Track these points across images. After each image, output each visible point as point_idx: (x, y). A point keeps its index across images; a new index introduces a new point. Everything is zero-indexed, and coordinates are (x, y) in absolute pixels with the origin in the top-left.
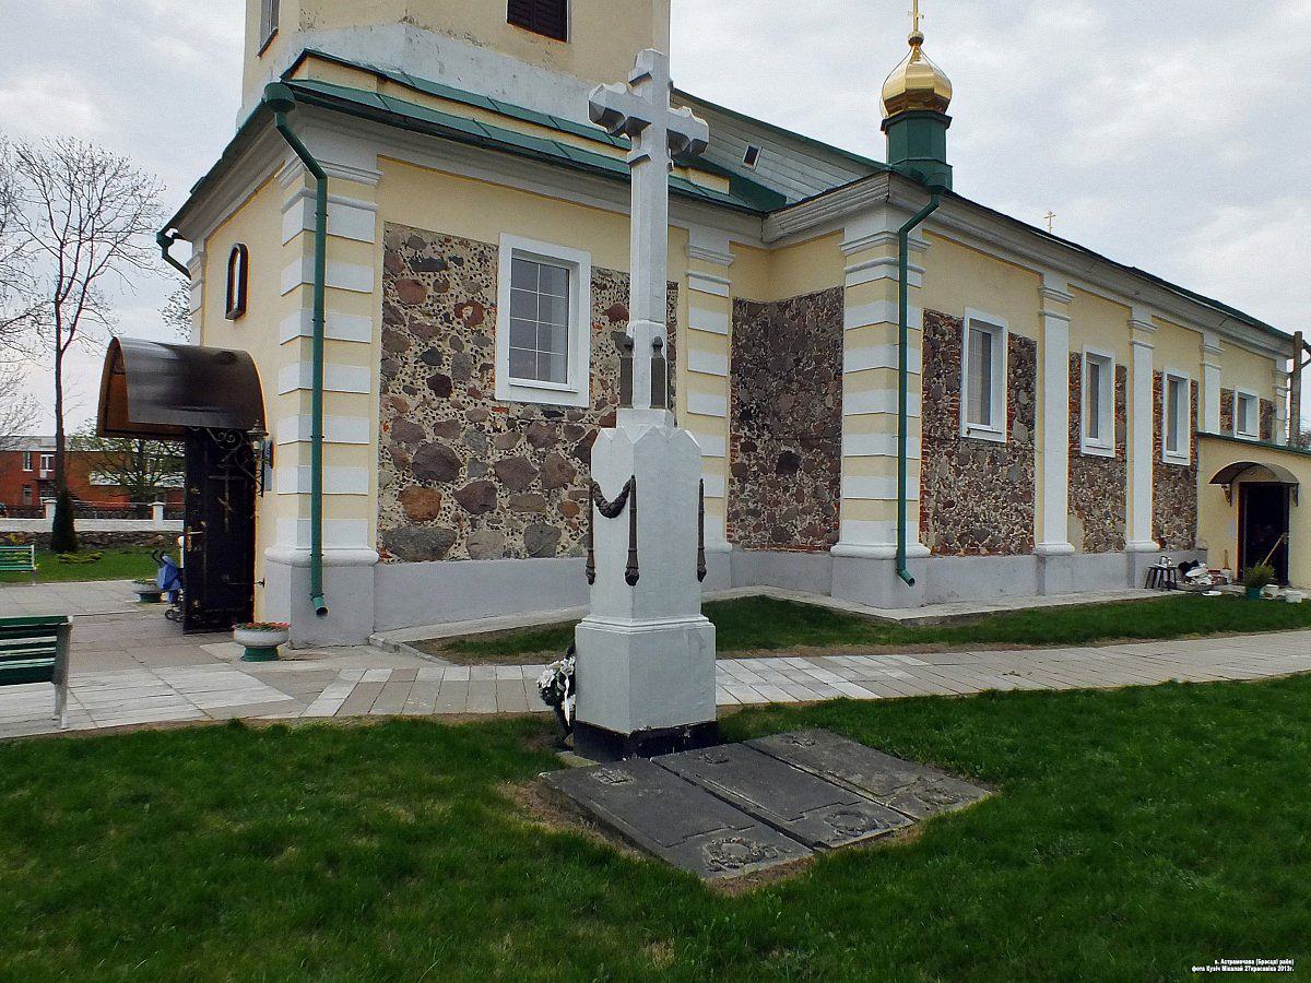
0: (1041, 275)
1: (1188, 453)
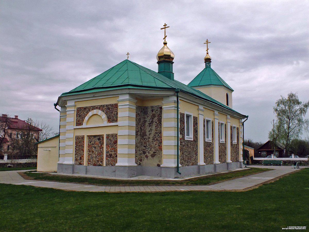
0: (214, 111)
1: (211, 139)
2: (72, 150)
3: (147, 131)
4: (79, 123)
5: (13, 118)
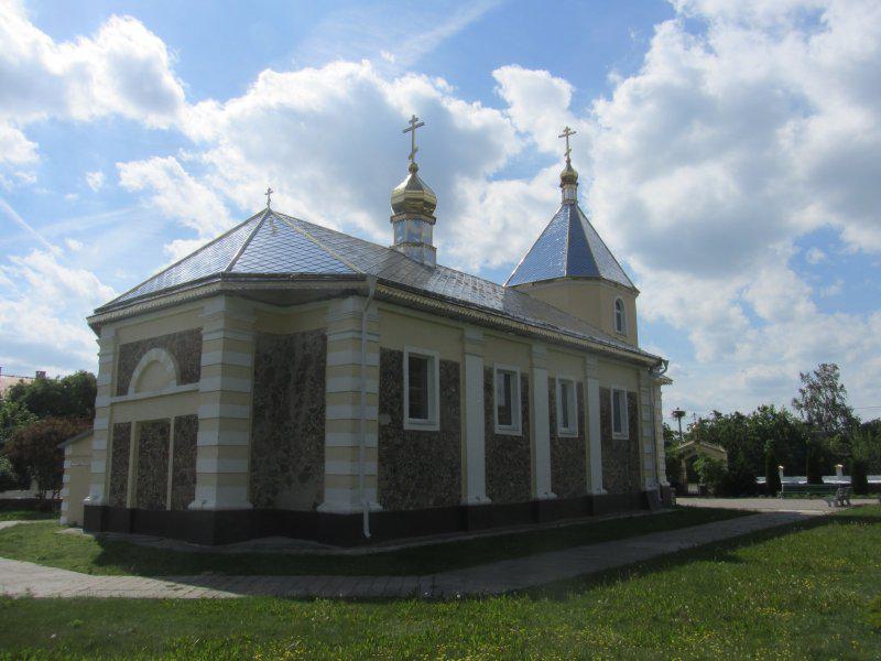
0: (462, 329)
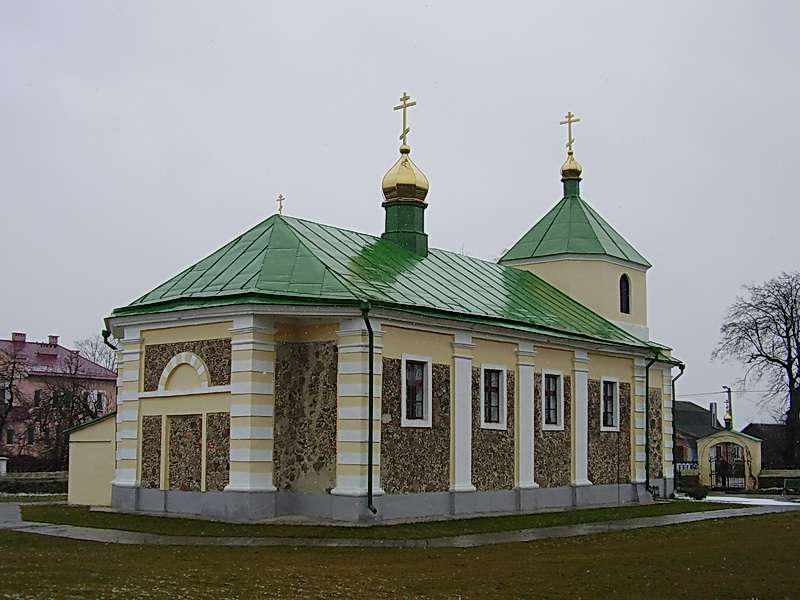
0: (517, 344)
2: (132, 452)
3: (306, 404)
4: (151, 386)
5: (42, 344)
